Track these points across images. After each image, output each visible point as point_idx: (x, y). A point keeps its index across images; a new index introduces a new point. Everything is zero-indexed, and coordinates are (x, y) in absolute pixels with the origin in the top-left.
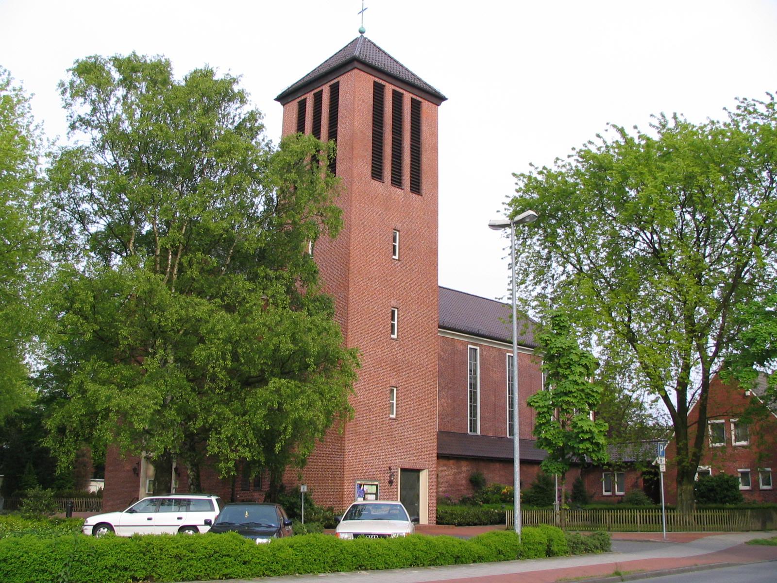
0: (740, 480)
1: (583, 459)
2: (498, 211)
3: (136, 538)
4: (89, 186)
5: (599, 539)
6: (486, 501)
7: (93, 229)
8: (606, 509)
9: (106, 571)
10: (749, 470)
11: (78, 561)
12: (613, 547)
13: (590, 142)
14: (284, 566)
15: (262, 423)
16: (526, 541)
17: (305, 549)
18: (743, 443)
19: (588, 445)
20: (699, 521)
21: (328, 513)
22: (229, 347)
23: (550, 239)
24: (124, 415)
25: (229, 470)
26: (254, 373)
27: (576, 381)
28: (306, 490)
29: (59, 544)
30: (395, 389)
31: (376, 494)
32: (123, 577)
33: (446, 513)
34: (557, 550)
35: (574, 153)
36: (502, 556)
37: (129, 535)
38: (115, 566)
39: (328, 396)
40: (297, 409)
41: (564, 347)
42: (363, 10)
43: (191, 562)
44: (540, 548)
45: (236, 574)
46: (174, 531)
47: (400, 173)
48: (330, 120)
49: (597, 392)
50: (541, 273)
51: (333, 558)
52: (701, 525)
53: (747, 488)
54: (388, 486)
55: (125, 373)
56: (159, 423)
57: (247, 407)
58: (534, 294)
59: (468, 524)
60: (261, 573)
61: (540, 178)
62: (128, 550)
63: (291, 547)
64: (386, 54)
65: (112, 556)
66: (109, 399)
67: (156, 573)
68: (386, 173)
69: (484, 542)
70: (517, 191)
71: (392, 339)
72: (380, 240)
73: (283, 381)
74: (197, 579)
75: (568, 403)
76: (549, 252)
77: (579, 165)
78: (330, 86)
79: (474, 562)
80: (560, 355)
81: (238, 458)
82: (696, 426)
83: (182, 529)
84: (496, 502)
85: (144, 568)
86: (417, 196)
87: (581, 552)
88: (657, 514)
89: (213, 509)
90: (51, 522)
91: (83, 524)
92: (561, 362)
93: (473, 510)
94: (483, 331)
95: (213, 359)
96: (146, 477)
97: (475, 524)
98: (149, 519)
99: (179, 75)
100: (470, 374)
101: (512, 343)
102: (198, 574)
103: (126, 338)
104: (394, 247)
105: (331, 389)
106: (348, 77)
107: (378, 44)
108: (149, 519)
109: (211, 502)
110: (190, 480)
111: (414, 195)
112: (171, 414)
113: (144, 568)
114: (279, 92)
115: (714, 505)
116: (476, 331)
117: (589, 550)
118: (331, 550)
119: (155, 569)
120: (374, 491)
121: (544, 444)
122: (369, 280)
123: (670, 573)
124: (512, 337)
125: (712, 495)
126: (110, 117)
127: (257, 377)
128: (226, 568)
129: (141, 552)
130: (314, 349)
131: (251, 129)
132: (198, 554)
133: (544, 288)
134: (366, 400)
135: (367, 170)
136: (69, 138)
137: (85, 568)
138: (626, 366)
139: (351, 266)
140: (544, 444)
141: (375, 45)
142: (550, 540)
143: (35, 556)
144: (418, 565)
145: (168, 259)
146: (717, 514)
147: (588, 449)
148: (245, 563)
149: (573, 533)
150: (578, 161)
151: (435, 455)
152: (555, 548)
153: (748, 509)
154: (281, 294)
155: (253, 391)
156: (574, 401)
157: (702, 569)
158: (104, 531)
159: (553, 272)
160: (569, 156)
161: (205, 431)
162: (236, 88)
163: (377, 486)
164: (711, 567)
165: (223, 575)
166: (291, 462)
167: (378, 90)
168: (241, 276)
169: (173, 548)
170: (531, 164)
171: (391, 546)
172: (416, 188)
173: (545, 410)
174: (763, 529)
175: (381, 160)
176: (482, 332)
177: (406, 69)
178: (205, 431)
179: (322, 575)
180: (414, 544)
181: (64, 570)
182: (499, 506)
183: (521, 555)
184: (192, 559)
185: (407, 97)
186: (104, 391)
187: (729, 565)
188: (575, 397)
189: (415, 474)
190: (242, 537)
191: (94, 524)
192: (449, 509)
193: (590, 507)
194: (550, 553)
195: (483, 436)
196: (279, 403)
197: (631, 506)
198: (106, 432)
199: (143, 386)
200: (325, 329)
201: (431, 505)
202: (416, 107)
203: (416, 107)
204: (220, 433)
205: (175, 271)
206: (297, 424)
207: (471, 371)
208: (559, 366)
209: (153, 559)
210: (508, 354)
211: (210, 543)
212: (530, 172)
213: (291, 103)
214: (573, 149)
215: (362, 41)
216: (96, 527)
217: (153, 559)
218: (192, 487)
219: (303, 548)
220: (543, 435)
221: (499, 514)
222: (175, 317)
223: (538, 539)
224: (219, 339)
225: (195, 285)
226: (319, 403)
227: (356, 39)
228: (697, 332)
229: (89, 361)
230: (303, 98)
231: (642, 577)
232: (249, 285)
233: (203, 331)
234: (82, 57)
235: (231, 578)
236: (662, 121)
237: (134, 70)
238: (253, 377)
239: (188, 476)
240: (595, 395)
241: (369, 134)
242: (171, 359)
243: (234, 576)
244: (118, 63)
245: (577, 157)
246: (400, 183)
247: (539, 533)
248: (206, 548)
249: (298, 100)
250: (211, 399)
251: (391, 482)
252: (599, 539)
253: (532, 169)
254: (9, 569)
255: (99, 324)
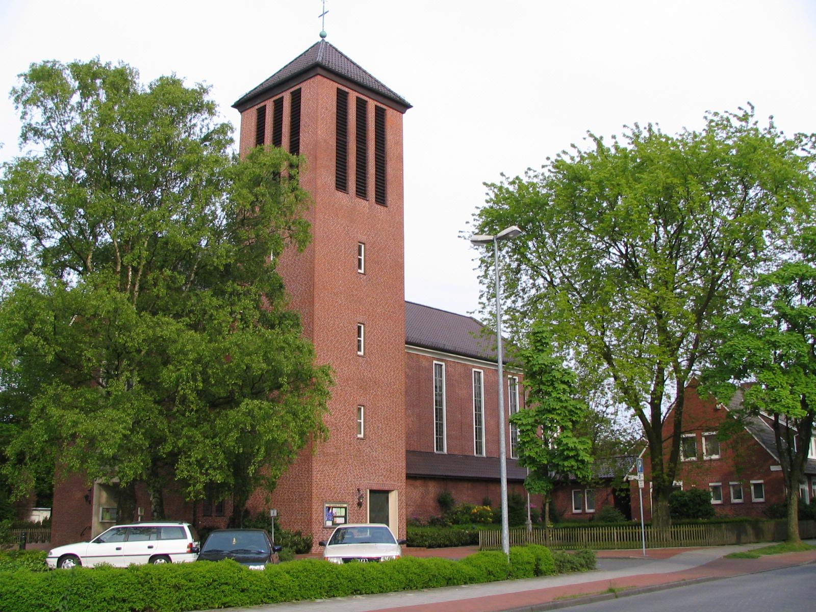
0: (712, 494)
1: (566, 477)
2: (467, 222)
3: (102, 568)
4: (46, 200)
5: (584, 558)
6: (456, 522)
7: (48, 243)
8: (572, 528)
9: (105, 604)
10: (720, 484)
11: (76, 594)
12: (598, 565)
13: (564, 152)
14: (282, 593)
15: (234, 447)
16: (515, 561)
17: (301, 575)
18: (715, 457)
19: (573, 463)
20: (675, 536)
21: (295, 538)
22: (199, 368)
23: (520, 251)
24: (92, 441)
25: (198, 493)
26: (223, 393)
27: (559, 398)
28: (275, 514)
29: (55, 577)
30: (362, 408)
31: (345, 517)
32: (122, 609)
33: (417, 535)
34: (545, 569)
35: (548, 163)
36: (492, 577)
37: (126, 566)
38: (114, 598)
39: (302, 417)
40: (272, 431)
41: (546, 363)
42: (324, 13)
43: (189, 592)
44: (528, 567)
45: (235, 602)
46: (145, 561)
47: (365, 184)
48: (291, 129)
49: (580, 409)
50: (512, 286)
51: (329, 583)
52: (677, 541)
53: (719, 502)
54: (357, 508)
55: (88, 396)
56: (127, 449)
57: (218, 430)
58: (505, 308)
59: (439, 546)
60: (259, 600)
61: (511, 188)
62: (126, 581)
63: (288, 573)
64: (348, 59)
65: (110, 588)
66: (75, 424)
67: (155, 604)
68: (350, 183)
69: (474, 562)
70: (487, 202)
71: (358, 356)
72: (345, 254)
73: (256, 402)
74: (196, 609)
75: (552, 421)
76: (519, 265)
77: (552, 175)
78: (292, 93)
79: (465, 583)
80: (541, 372)
81: (208, 481)
82: (670, 441)
83: (153, 558)
84: (466, 522)
85: (143, 600)
86: (382, 208)
87: (567, 571)
88: (634, 530)
89: (185, 537)
90: (9, 555)
91: (46, 556)
92: (544, 379)
93: (444, 531)
94: (449, 346)
95: (183, 380)
96: (99, 505)
97: (446, 546)
98: (118, 549)
99: (144, 83)
100: (436, 391)
101: (497, 362)
102: (197, 603)
103: (89, 360)
104: (360, 260)
105: (305, 409)
106: (310, 84)
107: (340, 49)
108: (118, 549)
109: (182, 529)
110: (153, 506)
111: (379, 207)
112: (139, 438)
113: (143, 600)
114: (237, 98)
115: (687, 520)
116: (441, 346)
117: (574, 568)
118: (326, 575)
119: (154, 599)
120: (343, 514)
121: (528, 462)
122: (335, 295)
123: (660, 588)
124: (497, 355)
125: (685, 510)
126: (68, 128)
127: (225, 398)
128: (225, 596)
129: (139, 583)
130: (288, 368)
131: (551, 189)
132: (196, 583)
133: (514, 302)
134: (333, 420)
135: (331, 180)
136: (21, 148)
137: (83, 601)
138: (600, 381)
139: (316, 280)
140: (528, 462)
141: (336, 50)
142: (538, 559)
143: (31, 591)
144: (411, 588)
145: (128, 276)
146: (694, 529)
147: (573, 466)
148: (243, 591)
149: (559, 552)
150: (549, 171)
151: (404, 476)
152: (543, 567)
153: (722, 523)
154: (250, 310)
155: (224, 412)
156: (558, 418)
157: (690, 583)
158: (70, 564)
159: (524, 285)
160: (543, 167)
161: (174, 456)
162: (206, 98)
163: (346, 508)
164: (698, 582)
165: (222, 604)
166: (261, 485)
167: (342, 97)
168: (208, 292)
169: (172, 577)
170: (502, 174)
171: (385, 570)
172: (381, 198)
173: (529, 427)
174: (738, 543)
175: (345, 170)
176: (447, 347)
177: (370, 76)
178: (174, 456)
179: (319, 600)
180: (408, 567)
181: (62, 603)
182: (470, 526)
183: (510, 575)
184: (191, 588)
185: (372, 105)
186: (71, 416)
187: (714, 579)
188: (559, 415)
189: (383, 496)
190: (238, 564)
191: (59, 555)
192: (419, 531)
193: (562, 525)
194: (538, 573)
195: (449, 455)
196: (252, 425)
197: (604, 523)
198: (69, 458)
199: (109, 410)
200: (298, 348)
201: (400, 527)
202: (380, 114)
203: (380, 114)
204: (190, 457)
205: (137, 289)
206: (271, 446)
207: (436, 387)
208: (542, 383)
209: (152, 589)
210: (474, 370)
211: (208, 571)
212: (501, 182)
213: (249, 111)
214: (548, 158)
215: (323, 46)
216: (62, 559)
217: (152, 589)
218: (155, 514)
219: (299, 574)
220: (527, 453)
221: (470, 535)
222: (142, 337)
223: (526, 559)
224: (188, 360)
225: (160, 303)
226: (292, 424)
227: (317, 44)
228: (670, 345)
229: (51, 384)
230: (262, 105)
231: (635, 593)
232: (215, 302)
233: (172, 350)
234: (39, 62)
235: (229, 606)
236: (636, 131)
237: (95, 76)
238: (221, 398)
239: (151, 503)
240: (578, 412)
241: (333, 143)
242: (136, 379)
243: (232, 605)
244: (76, 68)
245: (551, 168)
246: (365, 194)
247: (526, 553)
248: (204, 577)
249: (257, 107)
250: (180, 422)
251: (360, 504)
252: (584, 558)
253: (503, 179)
254: (5, 605)
255: (60, 345)
